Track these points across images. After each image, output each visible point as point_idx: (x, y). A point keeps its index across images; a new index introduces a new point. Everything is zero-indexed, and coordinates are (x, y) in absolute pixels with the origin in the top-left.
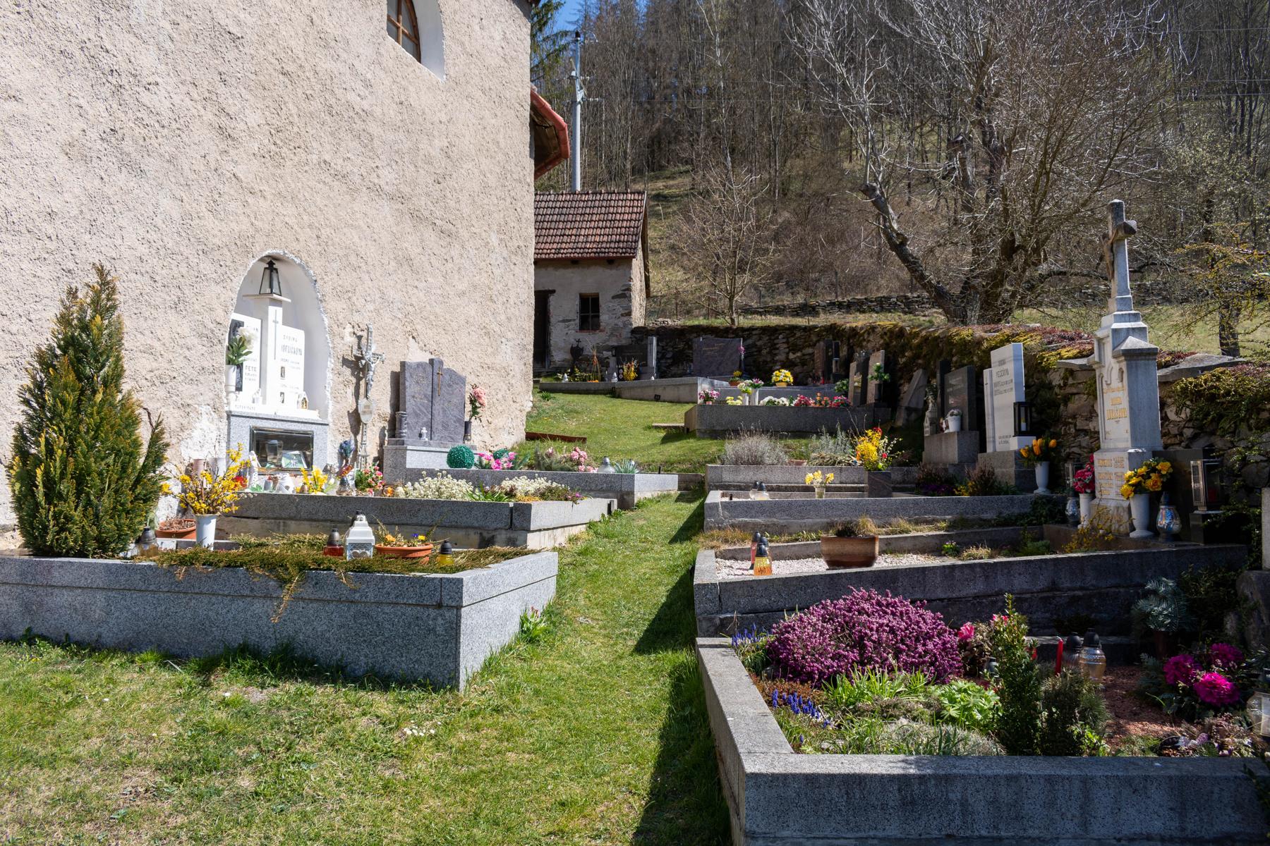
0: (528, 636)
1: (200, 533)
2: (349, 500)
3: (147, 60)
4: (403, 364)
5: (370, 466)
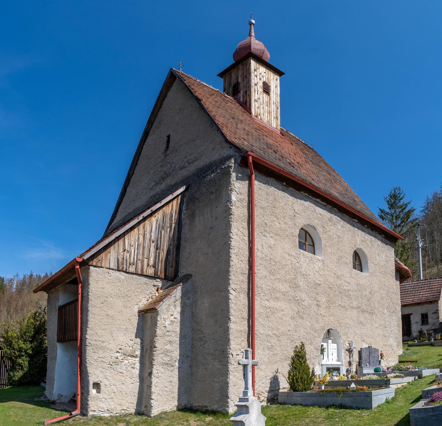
0: (387, 402)
1: (321, 388)
2: (350, 381)
3: (303, 296)
4: (361, 349)
5: (354, 373)
